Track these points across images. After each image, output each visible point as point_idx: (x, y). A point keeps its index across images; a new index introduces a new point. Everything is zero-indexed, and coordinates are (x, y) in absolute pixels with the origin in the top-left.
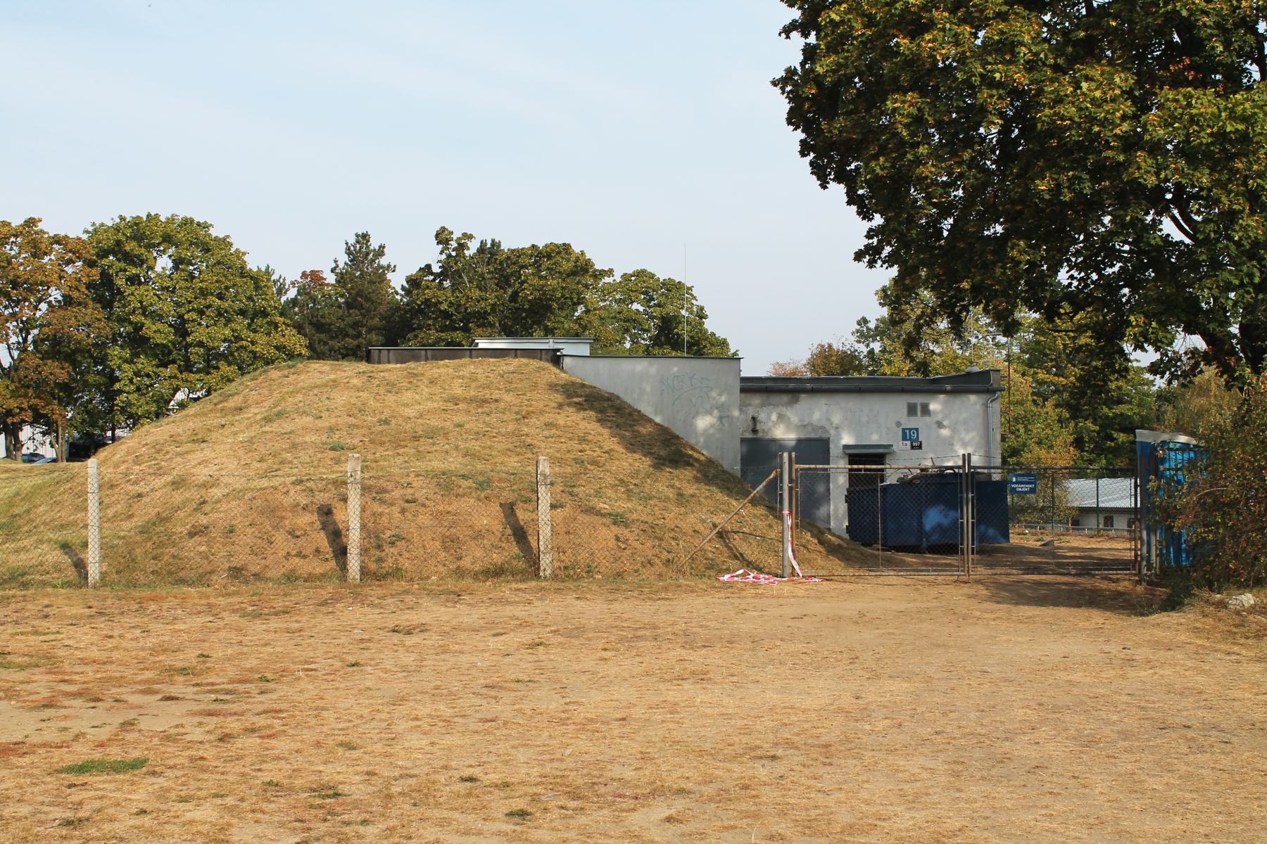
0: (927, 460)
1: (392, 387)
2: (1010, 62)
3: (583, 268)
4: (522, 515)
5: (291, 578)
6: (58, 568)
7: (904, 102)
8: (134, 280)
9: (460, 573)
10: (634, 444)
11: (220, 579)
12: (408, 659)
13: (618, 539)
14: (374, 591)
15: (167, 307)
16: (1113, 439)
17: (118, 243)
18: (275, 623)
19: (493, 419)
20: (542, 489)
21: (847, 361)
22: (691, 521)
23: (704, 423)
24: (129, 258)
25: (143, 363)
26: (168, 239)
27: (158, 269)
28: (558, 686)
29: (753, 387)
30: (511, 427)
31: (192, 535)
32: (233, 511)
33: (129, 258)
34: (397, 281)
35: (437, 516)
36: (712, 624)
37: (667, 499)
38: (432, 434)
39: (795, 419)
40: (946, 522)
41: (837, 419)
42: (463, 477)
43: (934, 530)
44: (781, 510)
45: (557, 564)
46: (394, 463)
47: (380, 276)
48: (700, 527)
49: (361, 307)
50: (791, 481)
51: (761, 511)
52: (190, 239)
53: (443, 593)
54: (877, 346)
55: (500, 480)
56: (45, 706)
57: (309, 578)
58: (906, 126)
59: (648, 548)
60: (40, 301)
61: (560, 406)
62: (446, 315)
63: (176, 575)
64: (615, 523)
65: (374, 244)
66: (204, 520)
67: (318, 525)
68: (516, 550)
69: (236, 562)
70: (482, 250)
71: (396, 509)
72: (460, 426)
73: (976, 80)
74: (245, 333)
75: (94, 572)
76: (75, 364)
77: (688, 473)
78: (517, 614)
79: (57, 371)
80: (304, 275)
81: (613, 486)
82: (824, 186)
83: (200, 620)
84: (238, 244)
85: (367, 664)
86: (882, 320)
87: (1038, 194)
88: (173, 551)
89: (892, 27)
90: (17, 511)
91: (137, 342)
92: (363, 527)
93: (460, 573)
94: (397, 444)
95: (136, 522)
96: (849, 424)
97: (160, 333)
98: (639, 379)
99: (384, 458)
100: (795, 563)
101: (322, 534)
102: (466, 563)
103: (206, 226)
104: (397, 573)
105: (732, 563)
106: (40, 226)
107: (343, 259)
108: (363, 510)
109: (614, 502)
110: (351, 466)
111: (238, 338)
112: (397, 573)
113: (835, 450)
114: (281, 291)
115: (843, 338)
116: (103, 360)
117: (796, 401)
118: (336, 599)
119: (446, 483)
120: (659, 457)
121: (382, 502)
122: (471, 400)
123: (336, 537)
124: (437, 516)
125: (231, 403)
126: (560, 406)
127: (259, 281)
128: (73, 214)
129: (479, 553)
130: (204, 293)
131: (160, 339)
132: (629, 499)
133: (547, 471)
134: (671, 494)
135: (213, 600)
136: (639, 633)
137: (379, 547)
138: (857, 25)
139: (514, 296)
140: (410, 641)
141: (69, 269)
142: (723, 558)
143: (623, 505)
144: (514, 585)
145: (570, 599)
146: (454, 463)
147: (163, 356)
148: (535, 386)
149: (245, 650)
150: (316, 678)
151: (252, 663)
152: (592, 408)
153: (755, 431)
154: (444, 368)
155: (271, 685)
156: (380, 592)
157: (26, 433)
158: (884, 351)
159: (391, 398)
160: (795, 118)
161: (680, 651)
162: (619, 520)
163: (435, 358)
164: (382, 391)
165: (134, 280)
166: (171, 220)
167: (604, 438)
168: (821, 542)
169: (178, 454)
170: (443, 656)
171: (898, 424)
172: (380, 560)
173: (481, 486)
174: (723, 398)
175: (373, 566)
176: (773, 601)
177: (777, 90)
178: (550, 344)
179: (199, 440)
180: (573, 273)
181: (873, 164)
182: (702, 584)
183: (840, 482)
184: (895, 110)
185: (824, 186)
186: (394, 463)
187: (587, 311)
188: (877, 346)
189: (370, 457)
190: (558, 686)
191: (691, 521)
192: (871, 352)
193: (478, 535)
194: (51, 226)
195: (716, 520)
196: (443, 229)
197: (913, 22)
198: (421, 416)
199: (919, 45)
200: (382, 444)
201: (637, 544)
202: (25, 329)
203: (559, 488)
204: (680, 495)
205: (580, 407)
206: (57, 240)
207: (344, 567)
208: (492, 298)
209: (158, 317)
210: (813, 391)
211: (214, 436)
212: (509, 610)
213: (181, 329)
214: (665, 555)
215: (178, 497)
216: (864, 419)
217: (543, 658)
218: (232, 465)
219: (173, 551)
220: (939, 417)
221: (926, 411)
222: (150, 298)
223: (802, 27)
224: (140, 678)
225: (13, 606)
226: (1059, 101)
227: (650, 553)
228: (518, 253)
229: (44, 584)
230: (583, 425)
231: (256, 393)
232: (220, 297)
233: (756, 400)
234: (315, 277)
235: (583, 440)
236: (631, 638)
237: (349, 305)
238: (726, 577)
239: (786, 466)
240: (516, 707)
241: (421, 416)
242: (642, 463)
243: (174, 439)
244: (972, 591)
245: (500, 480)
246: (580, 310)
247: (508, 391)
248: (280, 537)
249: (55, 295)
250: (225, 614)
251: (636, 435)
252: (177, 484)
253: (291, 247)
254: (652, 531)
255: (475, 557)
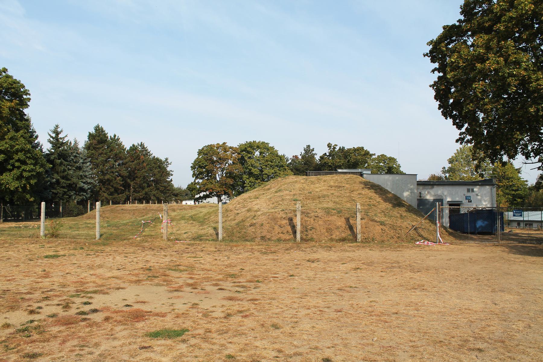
0: (472, 206)
1: (312, 183)
2: (519, 68)
3: (367, 153)
4: (351, 222)
5: (279, 240)
6: (211, 235)
7: (479, 85)
8: (249, 158)
9: (332, 240)
10: (386, 200)
11: (258, 240)
12: (311, 274)
13: (382, 230)
14: (304, 245)
15: (257, 165)
16: (516, 200)
17: (246, 148)
18: (270, 256)
19: (342, 192)
20: (358, 214)
21: (440, 178)
22: (405, 224)
23: (406, 194)
24: (248, 152)
25: (252, 179)
26: (258, 147)
27: (256, 155)
28: (366, 290)
29: (421, 184)
30: (348, 194)
31: (250, 226)
32: (262, 219)
33: (248, 152)
34: (317, 158)
35: (325, 222)
36: (419, 262)
37: (397, 217)
38: (324, 196)
39: (433, 193)
40: (483, 225)
41: (445, 193)
42: (333, 209)
43: (480, 227)
44: (436, 221)
45: (363, 237)
46: (312, 205)
47: (313, 156)
48: (408, 226)
49: (308, 165)
50: (439, 212)
51: (427, 221)
52: (264, 147)
53: (326, 247)
54: (447, 175)
55: (345, 210)
56: (176, 291)
57: (285, 240)
58: (480, 93)
59: (392, 233)
60: (226, 163)
61: (363, 188)
62: (330, 166)
63: (245, 238)
64: (381, 225)
65: (311, 148)
66: (254, 221)
67: (288, 224)
68: (349, 233)
69: (263, 235)
70: (340, 149)
71: (312, 219)
72: (333, 194)
73: (506, 75)
74: (277, 171)
75: (220, 237)
76: (235, 180)
77: (403, 209)
78: (350, 255)
79: (230, 181)
80: (293, 156)
81: (380, 213)
82: (446, 119)
83: (247, 254)
84: (276, 148)
85: (296, 276)
86: (450, 168)
87: (530, 113)
88: (245, 230)
89: (474, 61)
90: (206, 217)
91: (250, 174)
92: (302, 225)
93: (332, 240)
94: (314, 199)
95: (236, 221)
96: (449, 195)
97: (256, 171)
98: (385, 180)
99: (309, 203)
100: (440, 239)
101: (289, 227)
102: (334, 237)
103: (268, 144)
104: (312, 240)
105: (419, 238)
106: (227, 144)
107: (303, 152)
108: (302, 219)
109: (380, 218)
110: (298, 205)
111: (276, 173)
112: (312, 240)
113: (445, 202)
114: (287, 161)
115: (438, 172)
116: (242, 178)
117: (433, 188)
118: (291, 248)
119: (328, 211)
120: (394, 204)
121: (308, 217)
122: (336, 186)
123: (293, 227)
124: (325, 222)
125: (267, 187)
126: (363, 188)
127: (281, 158)
128: (234, 142)
129: (338, 233)
130: (267, 161)
131: (256, 173)
132: (385, 217)
133: (360, 208)
134: (398, 215)
135: (254, 247)
136: (394, 265)
137: (307, 231)
138: (461, 62)
139: (349, 161)
140: (313, 265)
141: (233, 155)
142: (416, 236)
143: (383, 219)
144: (349, 244)
145: (368, 250)
146: (331, 205)
147: (257, 177)
148: (355, 183)
149: (257, 267)
150: (276, 281)
151: (257, 273)
152: (372, 189)
153: (420, 197)
154: (328, 177)
155: (260, 284)
156: (306, 246)
157: (223, 197)
158: (450, 176)
159: (312, 186)
160: (436, 98)
161: (409, 273)
162: (382, 223)
163: (326, 174)
164: (310, 184)
165: (249, 158)
166: (259, 142)
167: (377, 198)
168: (446, 231)
169: (250, 202)
170: (323, 273)
171: (464, 195)
172: (307, 235)
173: (339, 212)
174: (412, 187)
175: (304, 237)
176: (437, 252)
177: (431, 88)
178: (360, 170)
179: (257, 198)
180: (364, 155)
181: (468, 106)
182: (410, 245)
183: (447, 212)
184: (476, 87)
185: (446, 119)
186: (312, 205)
187: (368, 165)
188: (447, 175)
189: (305, 203)
190: (366, 290)
191: (405, 224)
192: (446, 176)
193: (338, 228)
194: (229, 144)
195: (414, 224)
196: (329, 143)
197: (481, 59)
198: (321, 191)
199: (485, 65)
200: (309, 199)
201: (388, 231)
202: (222, 171)
203: (363, 213)
204: (401, 216)
205: (369, 189)
206: (231, 148)
207: (295, 237)
208: (342, 161)
209: (255, 167)
210: (438, 185)
211: (261, 197)
212: (347, 254)
213: (261, 171)
214: (397, 235)
215: (248, 214)
216: (454, 193)
217: (359, 275)
218: (264, 205)
219: (245, 230)
220: (477, 193)
221: (473, 191)
222: (253, 162)
223: (439, 70)
224: (218, 278)
225: (194, 247)
226: (538, 80)
227: (392, 234)
228: (349, 150)
229: (207, 240)
230: (370, 194)
231: (273, 185)
232: (271, 162)
233: (421, 187)
234: (296, 157)
235: (370, 198)
236: (391, 267)
237: (305, 164)
238: (418, 243)
239: (438, 207)
240: (350, 302)
241: (321, 191)
242: (389, 206)
243: (250, 198)
244: (502, 249)
245: (345, 210)
246: (366, 165)
247: (347, 184)
248: (276, 227)
249: (230, 162)
250: (255, 252)
251: (387, 197)
252: (249, 211)
253: (290, 149)
254: (393, 227)
255: (336, 235)
